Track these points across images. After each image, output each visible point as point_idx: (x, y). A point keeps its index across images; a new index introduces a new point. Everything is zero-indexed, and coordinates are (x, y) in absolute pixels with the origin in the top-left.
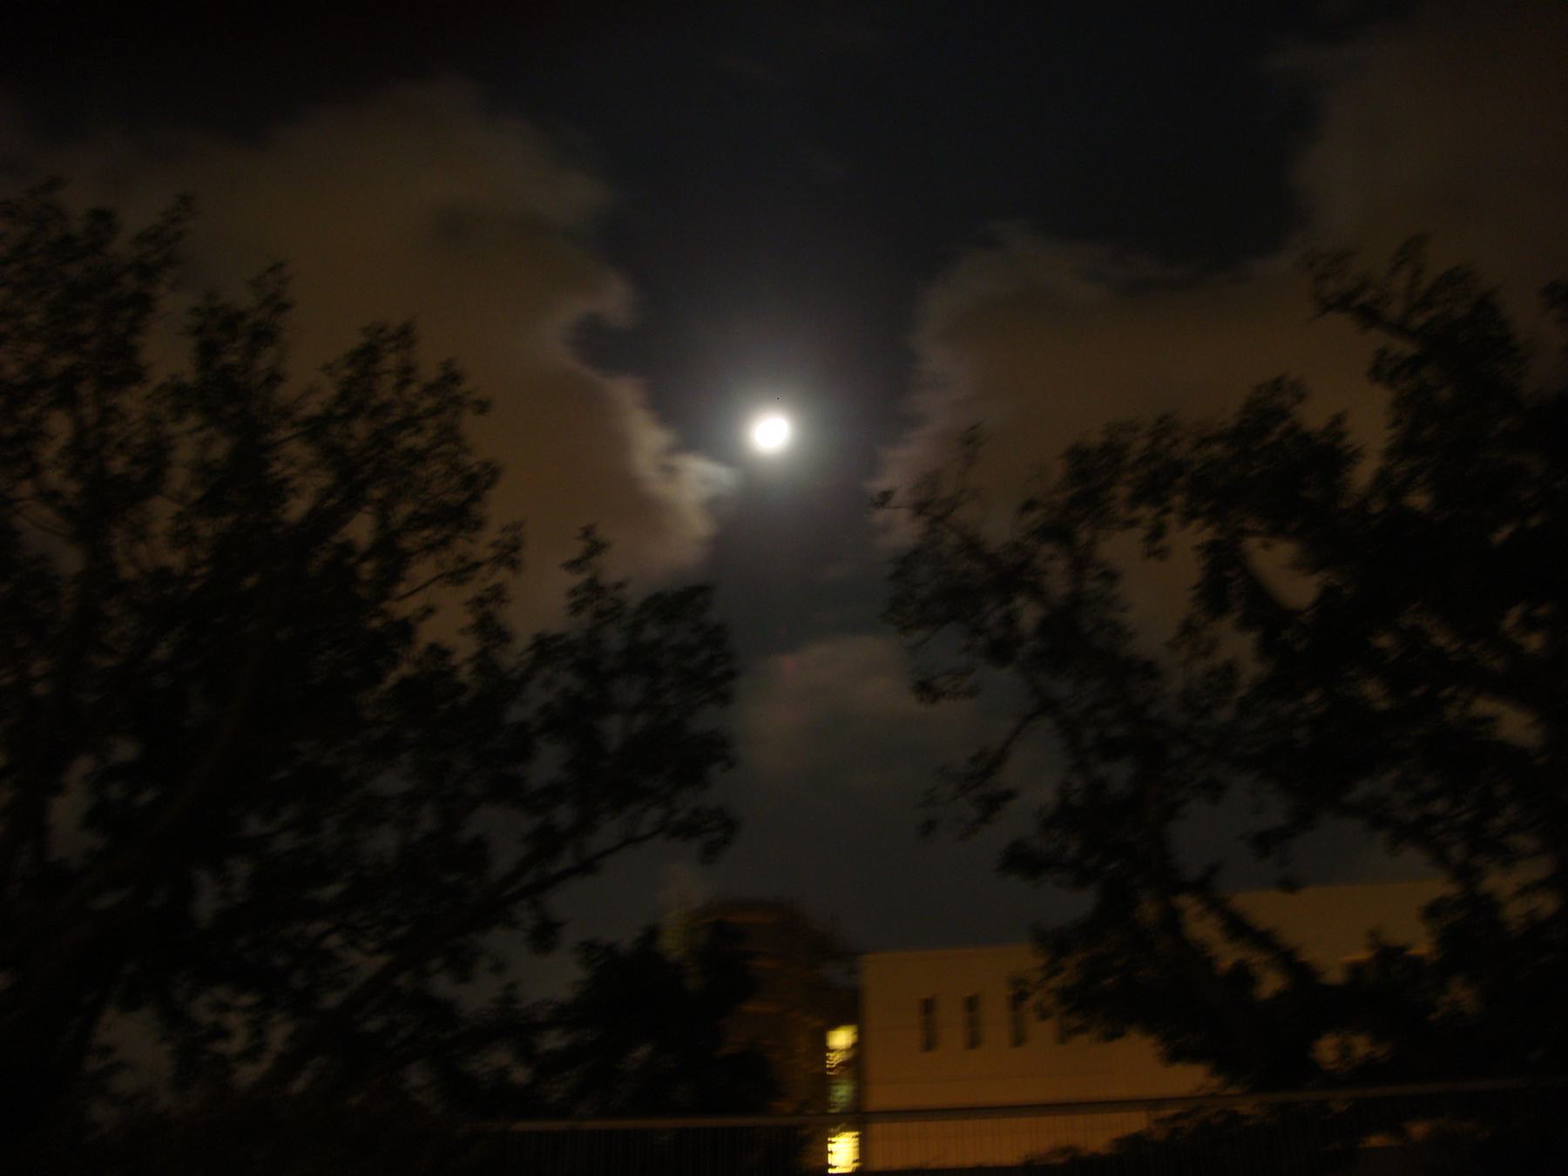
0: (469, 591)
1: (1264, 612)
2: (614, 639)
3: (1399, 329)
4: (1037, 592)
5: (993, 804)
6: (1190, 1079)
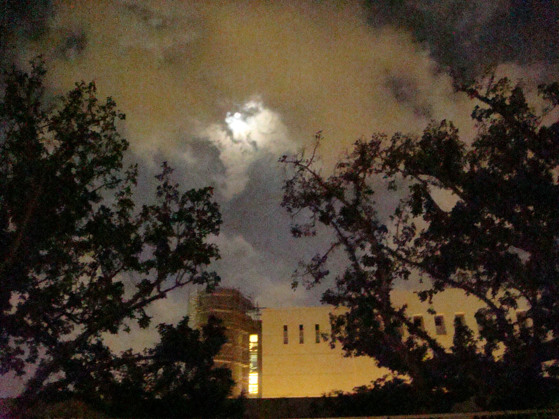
0: (117, 190)
1: (434, 212)
2: (174, 207)
3: (485, 100)
4: (340, 196)
5: (319, 276)
6: (384, 371)
